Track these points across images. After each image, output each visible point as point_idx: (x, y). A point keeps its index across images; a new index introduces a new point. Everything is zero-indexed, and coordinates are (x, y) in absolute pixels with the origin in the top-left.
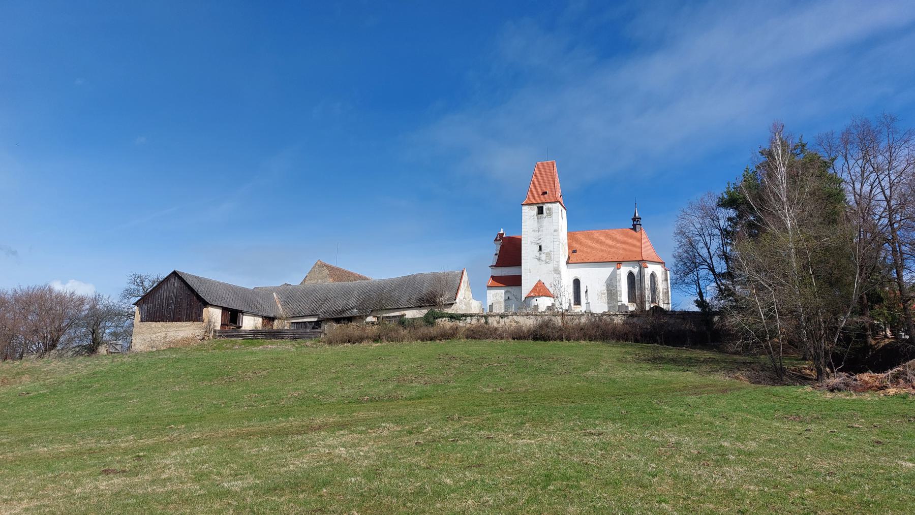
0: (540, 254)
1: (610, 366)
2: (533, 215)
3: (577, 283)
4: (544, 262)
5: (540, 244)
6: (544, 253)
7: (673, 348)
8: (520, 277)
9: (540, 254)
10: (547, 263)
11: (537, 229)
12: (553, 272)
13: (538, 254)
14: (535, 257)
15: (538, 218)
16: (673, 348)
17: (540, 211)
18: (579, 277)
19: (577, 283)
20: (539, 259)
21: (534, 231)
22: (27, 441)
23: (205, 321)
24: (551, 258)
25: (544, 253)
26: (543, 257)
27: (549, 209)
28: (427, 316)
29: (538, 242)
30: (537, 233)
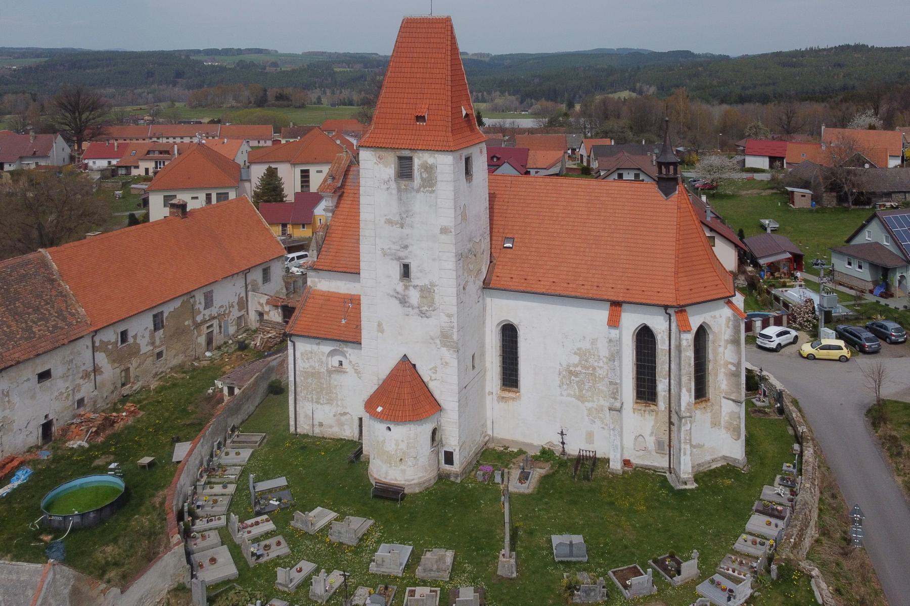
0: (406, 287)
1: (640, 504)
2: (386, 177)
3: (509, 334)
4: (416, 311)
5: (406, 261)
6: (415, 287)
7: (469, 454)
8: (309, 175)
9: (406, 287)
10: (422, 314)
11: (397, 218)
12: (438, 341)
13: (400, 287)
14: (392, 293)
15: (399, 190)
16: (469, 454)
17: (405, 170)
18: (514, 321)
19: (509, 334)
20: (404, 301)
21: (389, 222)
22: (211, 520)
23: (675, 424)
24: (433, 303)
25: (415, 287)
26: (414, 296)
27: (429, 169)
28: (91, 463)
29: (402, 254)
30: (396, 231)
